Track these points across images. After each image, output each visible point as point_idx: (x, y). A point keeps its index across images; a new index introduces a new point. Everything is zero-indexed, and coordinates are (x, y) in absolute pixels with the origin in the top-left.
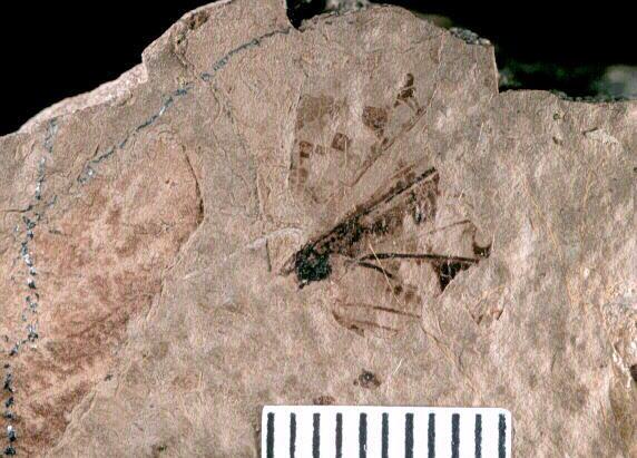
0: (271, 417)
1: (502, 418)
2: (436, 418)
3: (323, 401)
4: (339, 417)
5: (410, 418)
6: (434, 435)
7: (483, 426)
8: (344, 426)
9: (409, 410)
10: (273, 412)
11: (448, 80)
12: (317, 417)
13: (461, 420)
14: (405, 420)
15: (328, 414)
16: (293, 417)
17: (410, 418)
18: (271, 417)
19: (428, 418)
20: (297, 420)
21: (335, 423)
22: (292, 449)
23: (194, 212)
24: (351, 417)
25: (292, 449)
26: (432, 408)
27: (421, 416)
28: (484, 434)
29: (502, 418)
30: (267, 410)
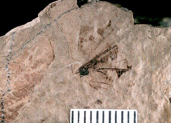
0: (73, 112)
1: (135, 112)
2: (117, 112)
3: (87, 108)
4: (91, 112)
5: (110, 112)
6: (116, 117)
7: (130, 114)
8: (92, 114)
9: (110, 110)
10: (73, 111)
11: (120, 21)
12: (85, 112)
13: (124, 113)
14: (109, 113)
15: (88, 111)
16: (79, 112)
17: (110, 112)
18: (73, 112)
19: (115, 112)
20: (80, 113)
21: (90, 114)
22: (78, 121)
23: (52, 57)
24: (94, 112)
25: (78, 121)
26: (116, 110)
27: (113, 112)
28: (130, 117)
29: (135, 112)
30: (72, 110)
